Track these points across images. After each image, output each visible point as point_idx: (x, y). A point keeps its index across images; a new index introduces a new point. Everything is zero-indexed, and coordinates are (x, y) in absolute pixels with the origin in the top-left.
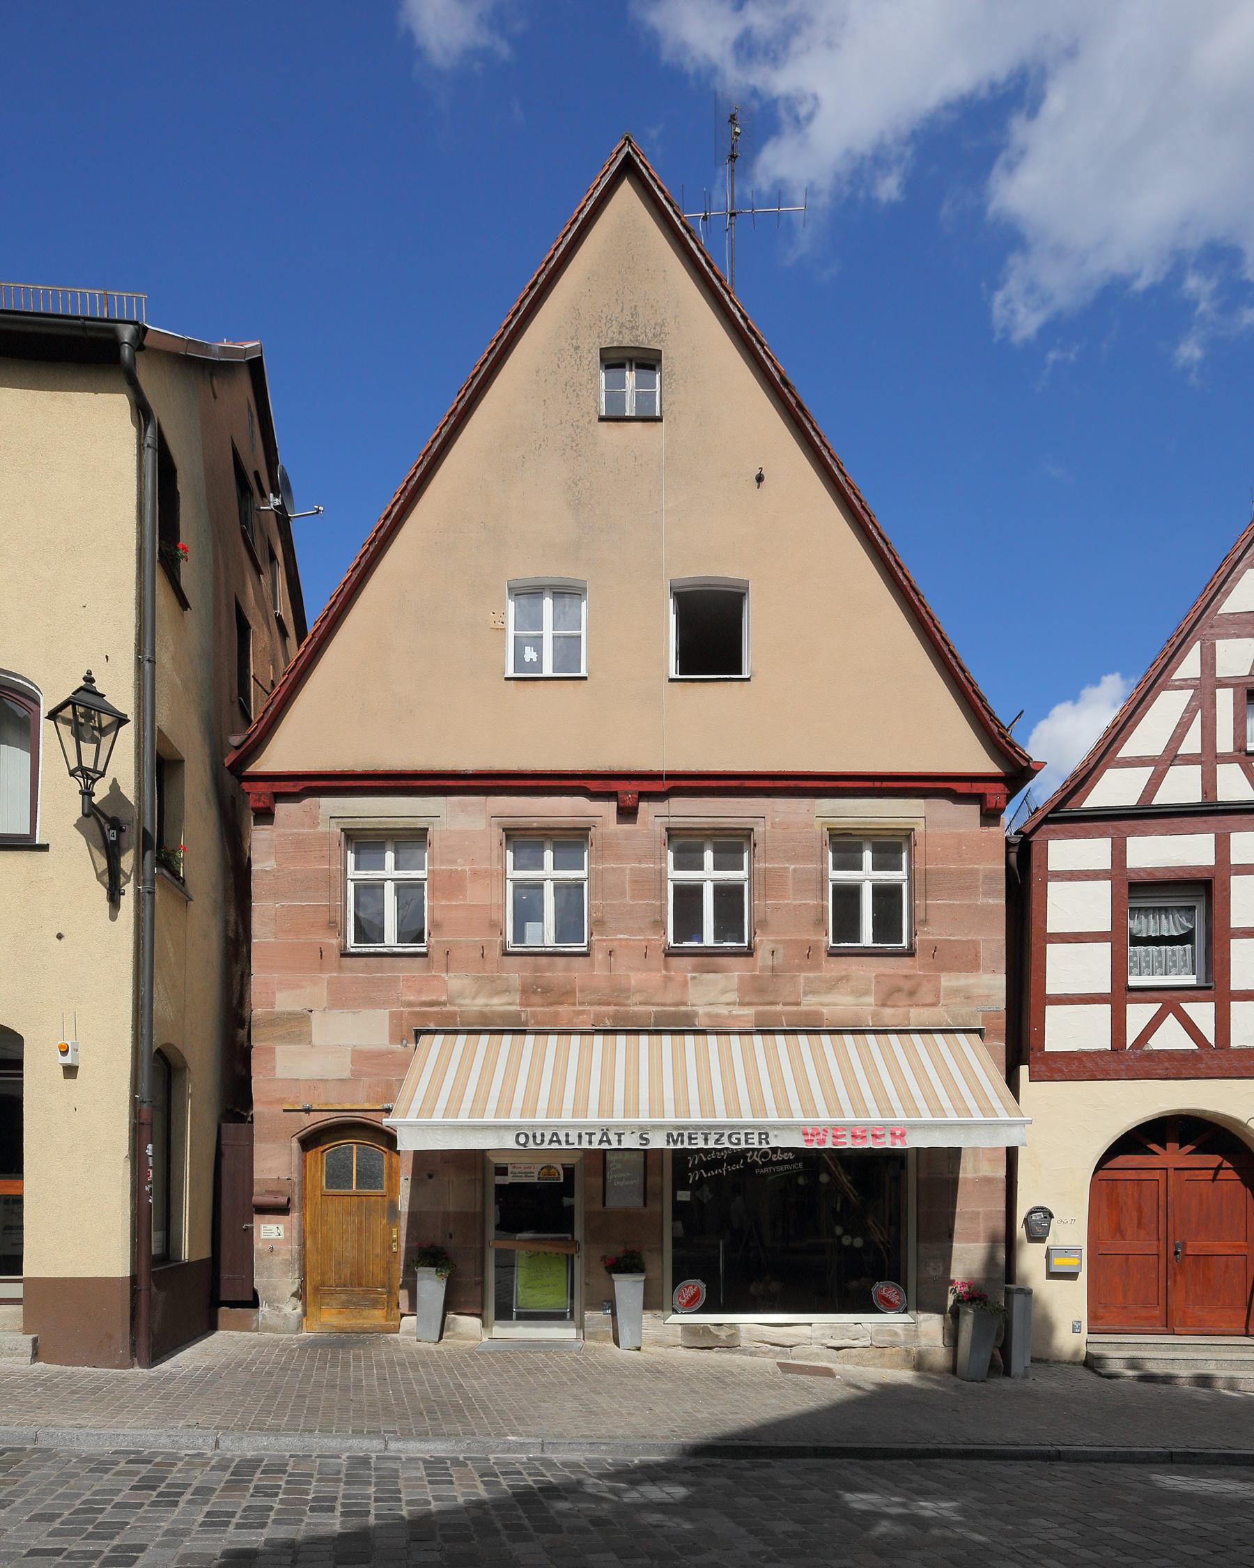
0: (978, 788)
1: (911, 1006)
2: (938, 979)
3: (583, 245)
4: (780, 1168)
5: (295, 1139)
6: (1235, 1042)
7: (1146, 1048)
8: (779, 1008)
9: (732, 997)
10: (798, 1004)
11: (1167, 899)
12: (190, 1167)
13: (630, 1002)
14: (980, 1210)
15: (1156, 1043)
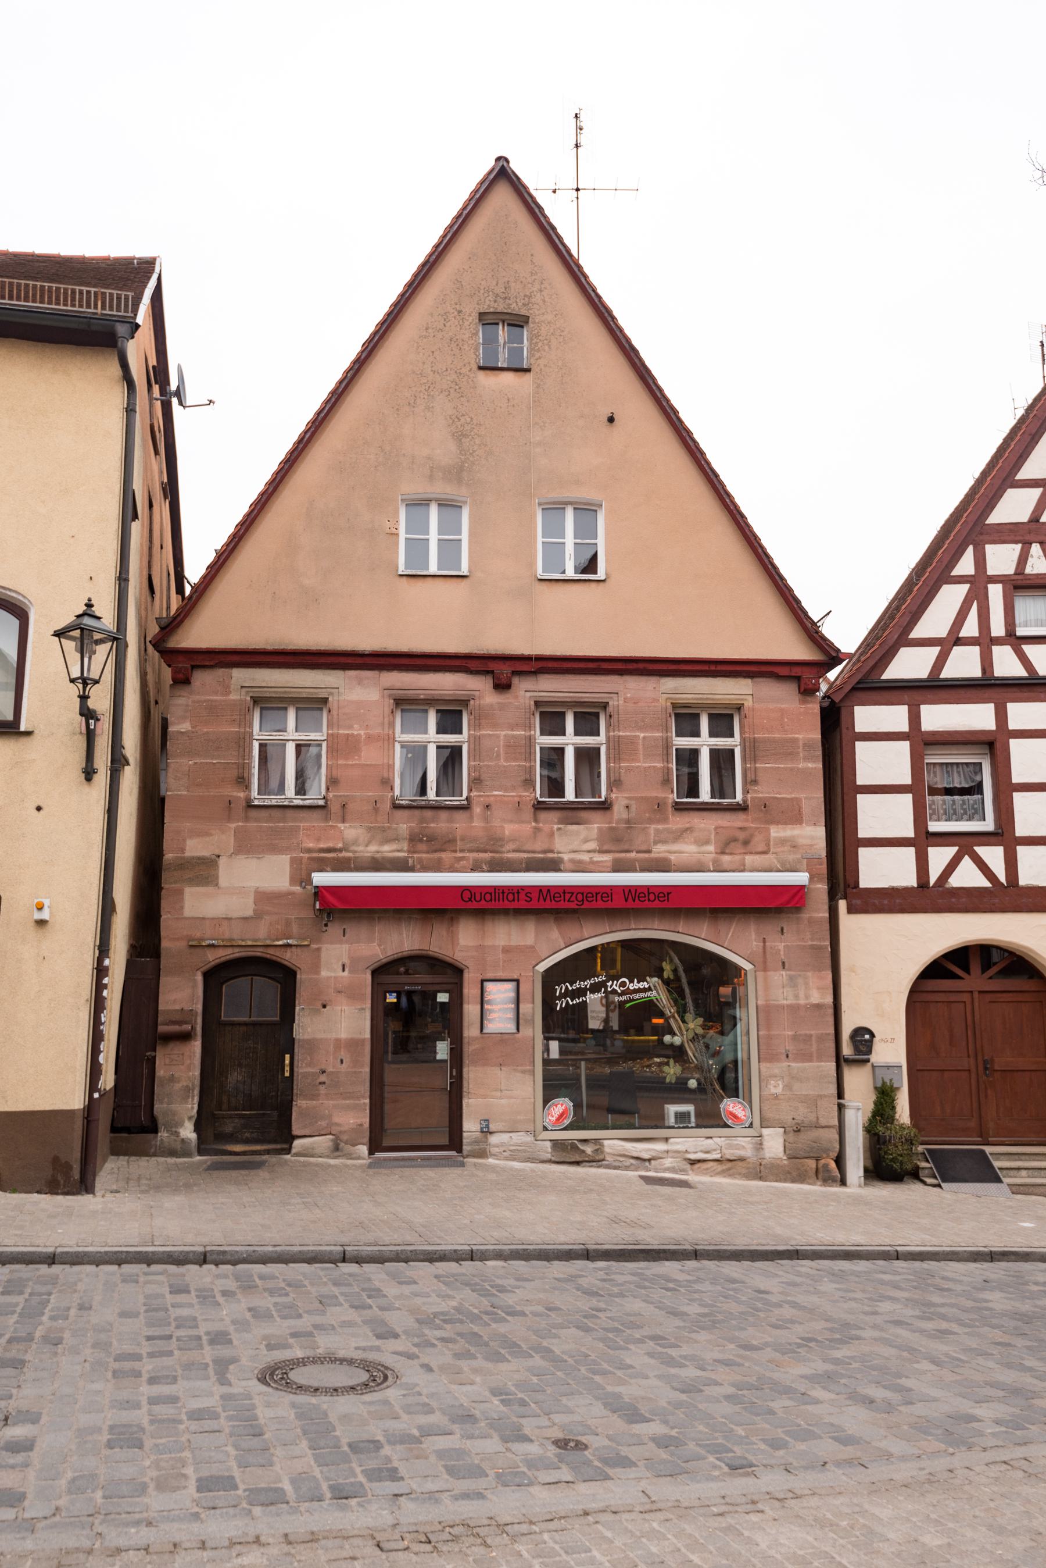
4: (637, 996)
8: (633, 855)
10: (649, 852)
13: (504, 849)
14: (813, 1032)
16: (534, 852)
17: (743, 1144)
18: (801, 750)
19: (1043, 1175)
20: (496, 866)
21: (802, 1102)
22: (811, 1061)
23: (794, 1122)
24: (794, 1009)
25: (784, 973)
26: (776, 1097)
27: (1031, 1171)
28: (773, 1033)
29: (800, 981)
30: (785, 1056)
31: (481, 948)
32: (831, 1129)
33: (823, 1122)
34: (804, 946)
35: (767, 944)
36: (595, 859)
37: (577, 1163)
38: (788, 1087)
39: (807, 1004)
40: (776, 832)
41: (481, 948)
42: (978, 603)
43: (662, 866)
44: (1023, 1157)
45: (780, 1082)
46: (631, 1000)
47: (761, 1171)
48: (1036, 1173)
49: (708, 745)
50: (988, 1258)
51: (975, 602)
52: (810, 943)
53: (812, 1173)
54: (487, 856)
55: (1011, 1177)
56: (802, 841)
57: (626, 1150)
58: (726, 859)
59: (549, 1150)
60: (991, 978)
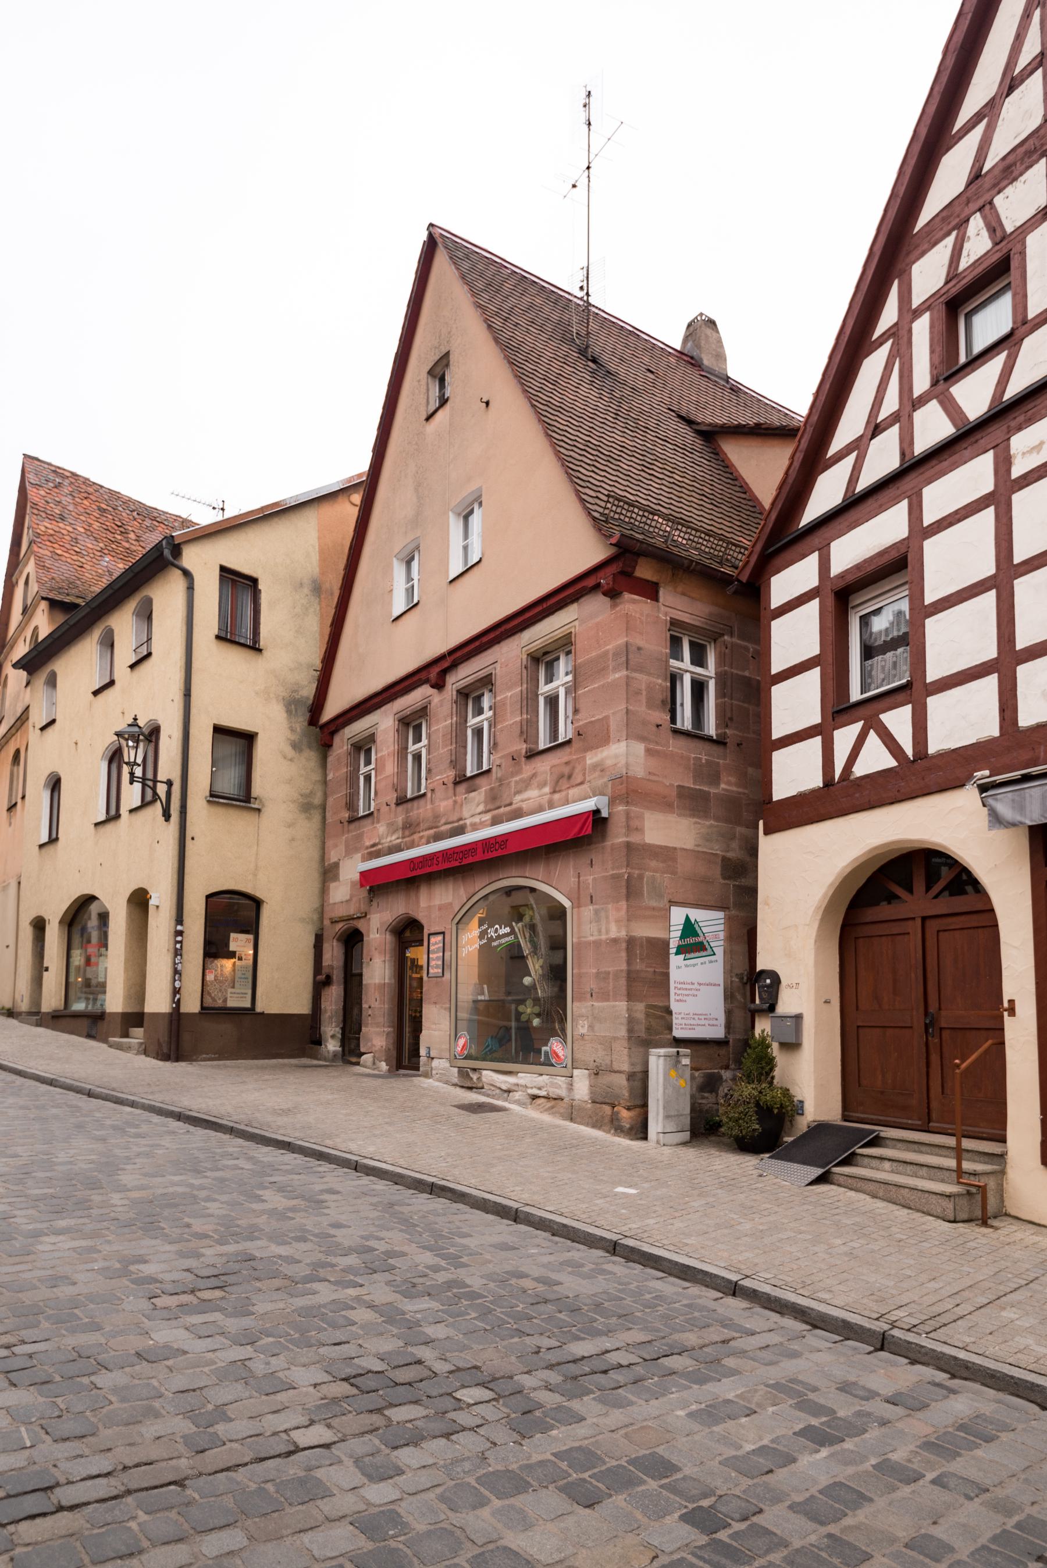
0: (590, 582)
1: (569, 788)
2: (584, 758)
3: (998, 14)
4: (503, 941)
5: (335, 941)
6: (934, 747)
7: (852, 777)
8: (502, 810)
9: (481, 808)
10: (511, 804)
11: (892, 593)
12: (977, 1059)
13: (440, 824)
14: (610, 969)
15: (860, 770)
16: (453, 822)
17: (560, 1083)
18: (610, 662)
19: (909, 1172)
20: (438, 837)
21: (601, 1044)
22: (608, 1000)
23: (596, 1064)
24: (597, 944)
25: (591, 907)
26: (582, 1036)
27: (895, 1164)
28: (584, 971)
29: (603, 914)
30: (589, 995)
31: (429, 907)
32: (622, 1075)
33: (616, 1067)
34: (607, 876)
35: (581, 878)
36: (483, 819)
37: (470, 1088)
38: (591, 1027)
39: (607, 939)
40: (592, 758)
41: (429, 907)
42: (900, 359)
43: (518, 814)
44: (924, 1148)
45: (586, 1022)
46: (500, 945)
47: (572, 1114)
48: (902, 1168)
49: (563, 685)
50: (428, 1189)
51: (898, 359)
52: (611, 872)
53: (607, 1120)
54: (432, 832)
55: (872, 1168)
56: (609, 762)
57: (493, 1080)
58: (557, 796)
59: (456, 1075)
60: (936, 897)
